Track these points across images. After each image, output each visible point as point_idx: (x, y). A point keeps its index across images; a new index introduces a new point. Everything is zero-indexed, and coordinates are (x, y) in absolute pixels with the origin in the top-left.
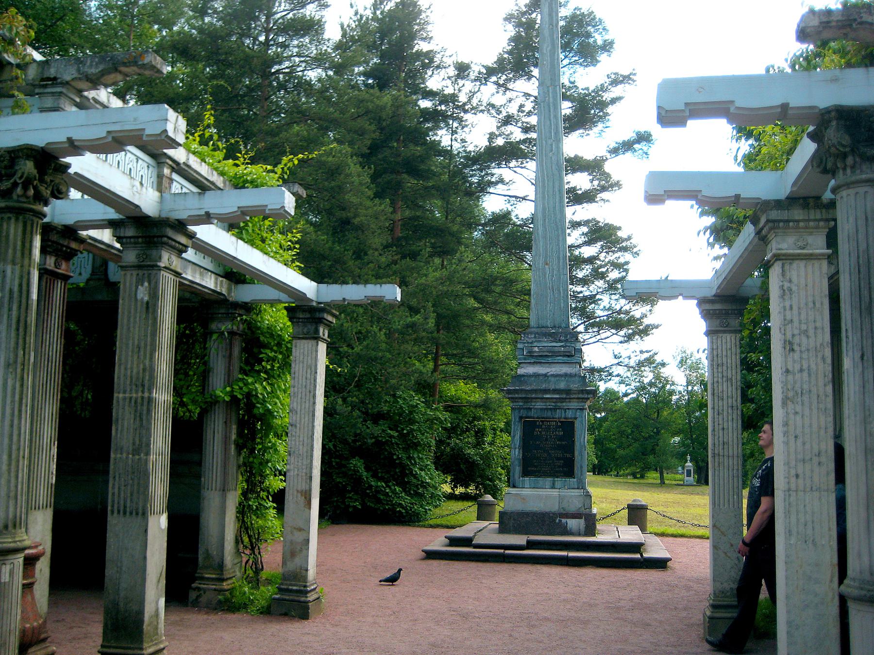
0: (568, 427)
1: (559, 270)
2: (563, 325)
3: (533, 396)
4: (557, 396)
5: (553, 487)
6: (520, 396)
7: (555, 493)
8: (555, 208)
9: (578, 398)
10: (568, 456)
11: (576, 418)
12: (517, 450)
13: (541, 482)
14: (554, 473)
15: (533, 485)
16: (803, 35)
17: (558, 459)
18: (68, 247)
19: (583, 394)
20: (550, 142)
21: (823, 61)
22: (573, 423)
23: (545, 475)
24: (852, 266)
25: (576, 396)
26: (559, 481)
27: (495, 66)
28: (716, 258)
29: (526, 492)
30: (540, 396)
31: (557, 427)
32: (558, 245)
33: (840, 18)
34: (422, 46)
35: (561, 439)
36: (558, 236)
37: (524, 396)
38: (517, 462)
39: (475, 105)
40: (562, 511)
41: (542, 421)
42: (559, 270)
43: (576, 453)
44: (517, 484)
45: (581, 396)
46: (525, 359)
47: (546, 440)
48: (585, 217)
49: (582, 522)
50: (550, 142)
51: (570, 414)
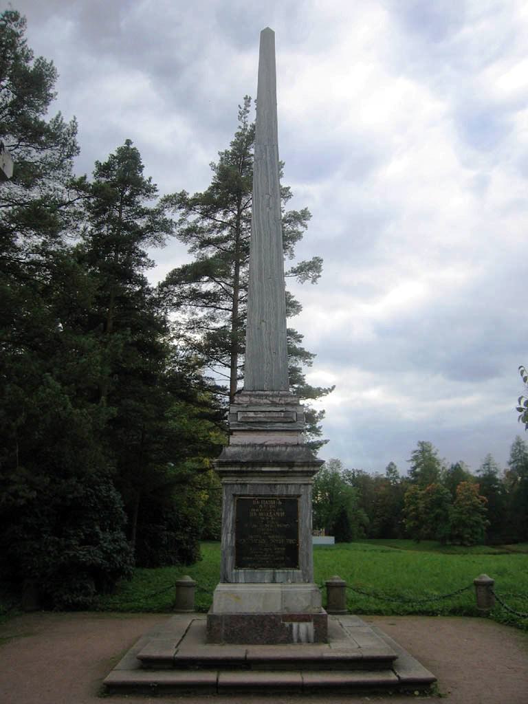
0: (291, 504)
3: (250, 469)
4: (278, 469)
5: (274, 581)
6: (234, 469)
7: (276, 589)
9: (302, 472)
10: (291, 541)
13: (259, 576)
14: (275, 564)
16: (41, 64)
17: (279, 545)
19: (308, 466)
21: (52, 552)
23: (264, 565)
24: (497, 551)
25: (300, 469)
26: (280, 574)
27: (209, 191)
29: (241, 588)
30: (258, 469)
31: (277, 506)
33: (509, 468)
34: (51, 91)
37: (238, 469)
38: (229, 551)
40: (286, 612)
43: (301, 539)
44: (229, 578)
45: (306, 469)
46: (238, 425)
47: (265, 522)
49: (310, 625)
51: (292, 491)
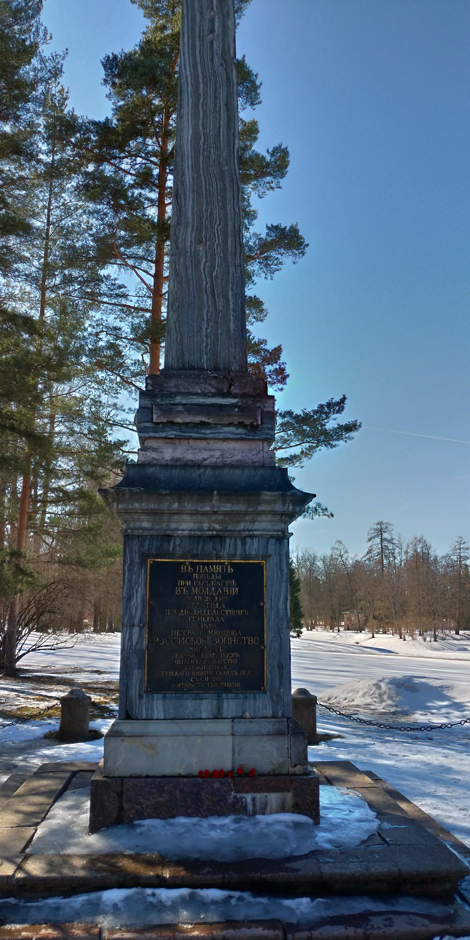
1: (225, 258)
2: (235, 367)
8: (217, 136)
11: (266, 557)
12: (136, 630)
14: (216, 686)
15: (172, 713)
18: (207, 361)
20: (208, 15)
22: (259, 568)
23: (200, 689)
28: (254, 337)
32: (224, 208)
35: (233, 602)
36: (224, 190)
39: (130, 166)
41: (193, 565)
42: (225, 258)
48: (60, 662)
50: (208, 15)
51: (253, 547)
